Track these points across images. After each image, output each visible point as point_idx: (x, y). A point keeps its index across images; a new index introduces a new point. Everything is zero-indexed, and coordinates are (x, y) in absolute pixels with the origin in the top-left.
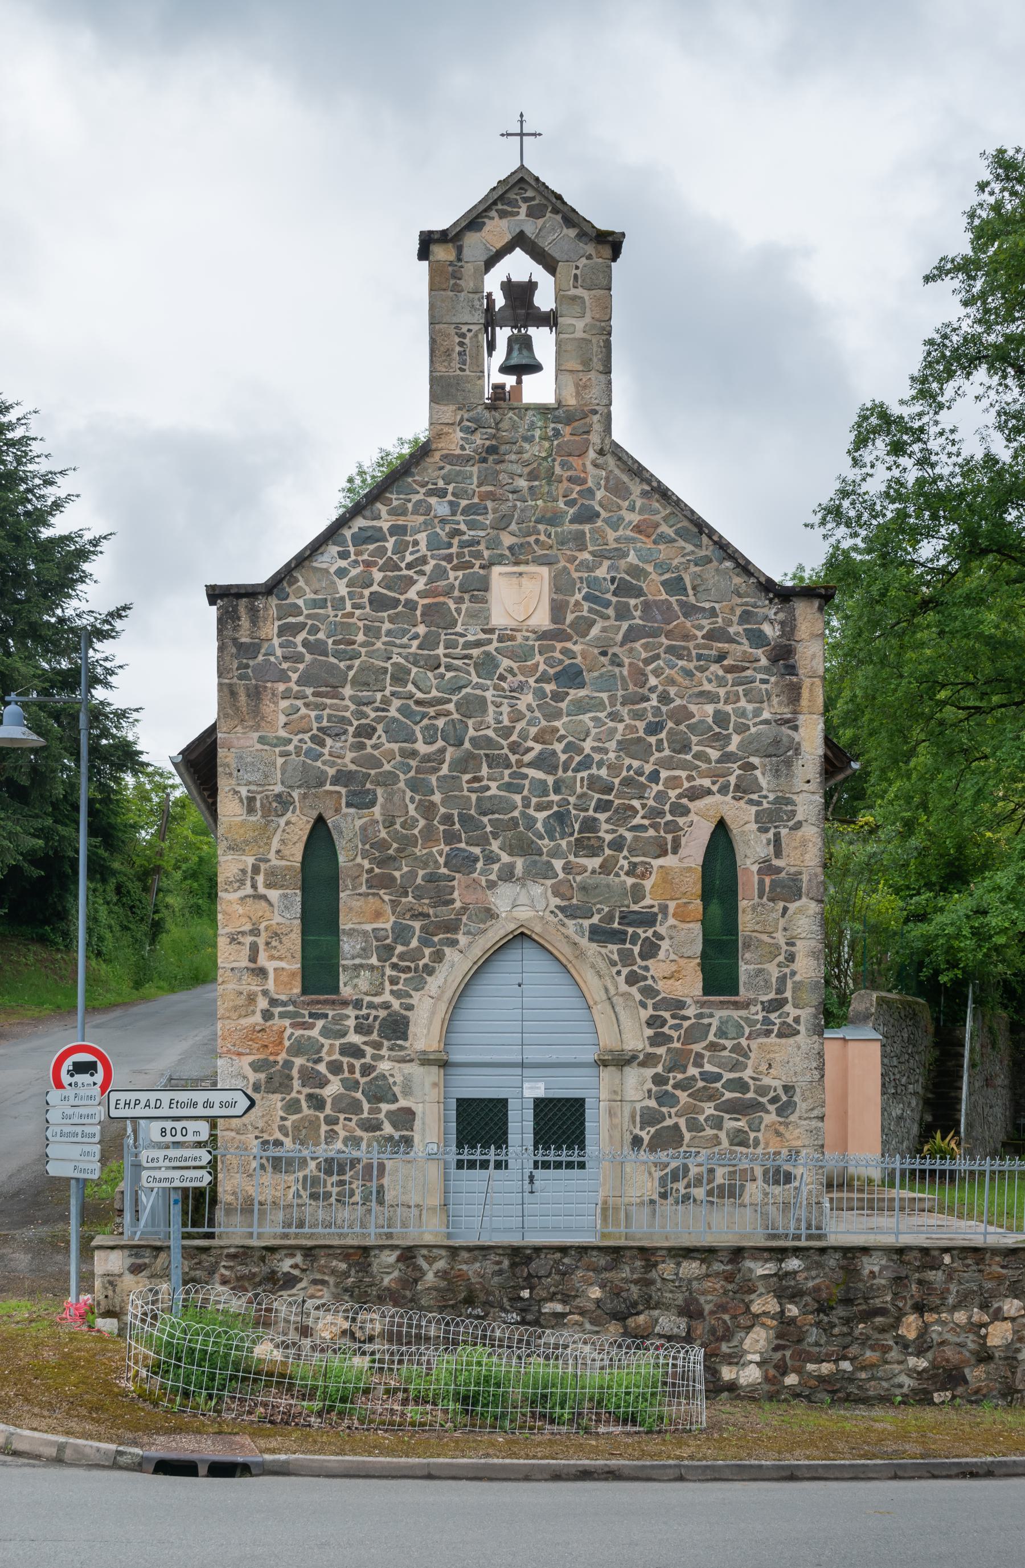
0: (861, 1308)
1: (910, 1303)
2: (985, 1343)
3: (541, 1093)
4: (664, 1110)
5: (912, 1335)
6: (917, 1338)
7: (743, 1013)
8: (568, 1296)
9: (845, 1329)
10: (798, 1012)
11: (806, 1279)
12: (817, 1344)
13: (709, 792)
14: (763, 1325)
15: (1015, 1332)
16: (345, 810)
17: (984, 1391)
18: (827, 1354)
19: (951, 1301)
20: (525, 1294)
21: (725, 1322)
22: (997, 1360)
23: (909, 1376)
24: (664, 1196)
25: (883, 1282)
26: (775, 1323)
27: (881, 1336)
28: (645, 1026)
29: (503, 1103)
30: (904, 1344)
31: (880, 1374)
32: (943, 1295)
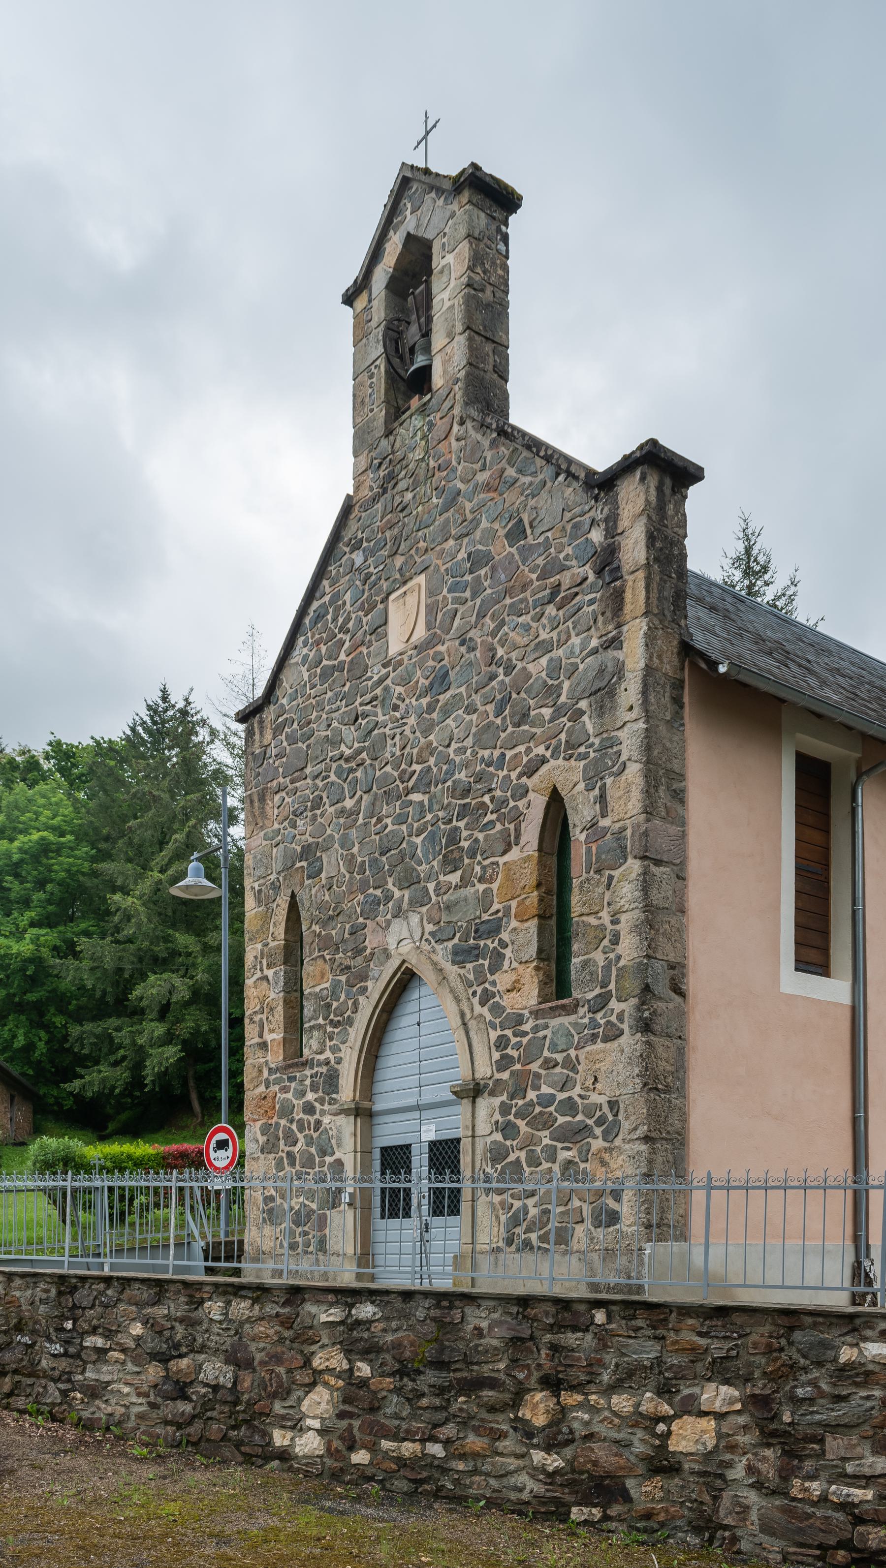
0: (458, 1375)
1: (536, 1375)
2: (663, 1447)
3: (432, 1136)
4: (508, 1143)
5: (540, 1421)
6: (549, 1426)
7: (572, 1018)
8: (111, 1331)
9: (437, 1402)
10: (623, 1006)
11: (384, 1330)
12: (397, 1416)
13: (543, 761)
14: (326, 1384)
15: (720, 1436)
16: (307, 882)
17: (662, 1517)
18: (407, 1431)
19: (606, 1377)
20: (69, 1325)
21: (278, 1376)
22: (686, 1475)
23: (533, 1477)
24: (510, 1242)
25: (495, 1343)
26: (341, 1383)
27: (490, 1417)
28: (493, 1049)
29: (408, 1147)
30: (527, 1432)
31: (487, 1468)
32: (593, 1367)
